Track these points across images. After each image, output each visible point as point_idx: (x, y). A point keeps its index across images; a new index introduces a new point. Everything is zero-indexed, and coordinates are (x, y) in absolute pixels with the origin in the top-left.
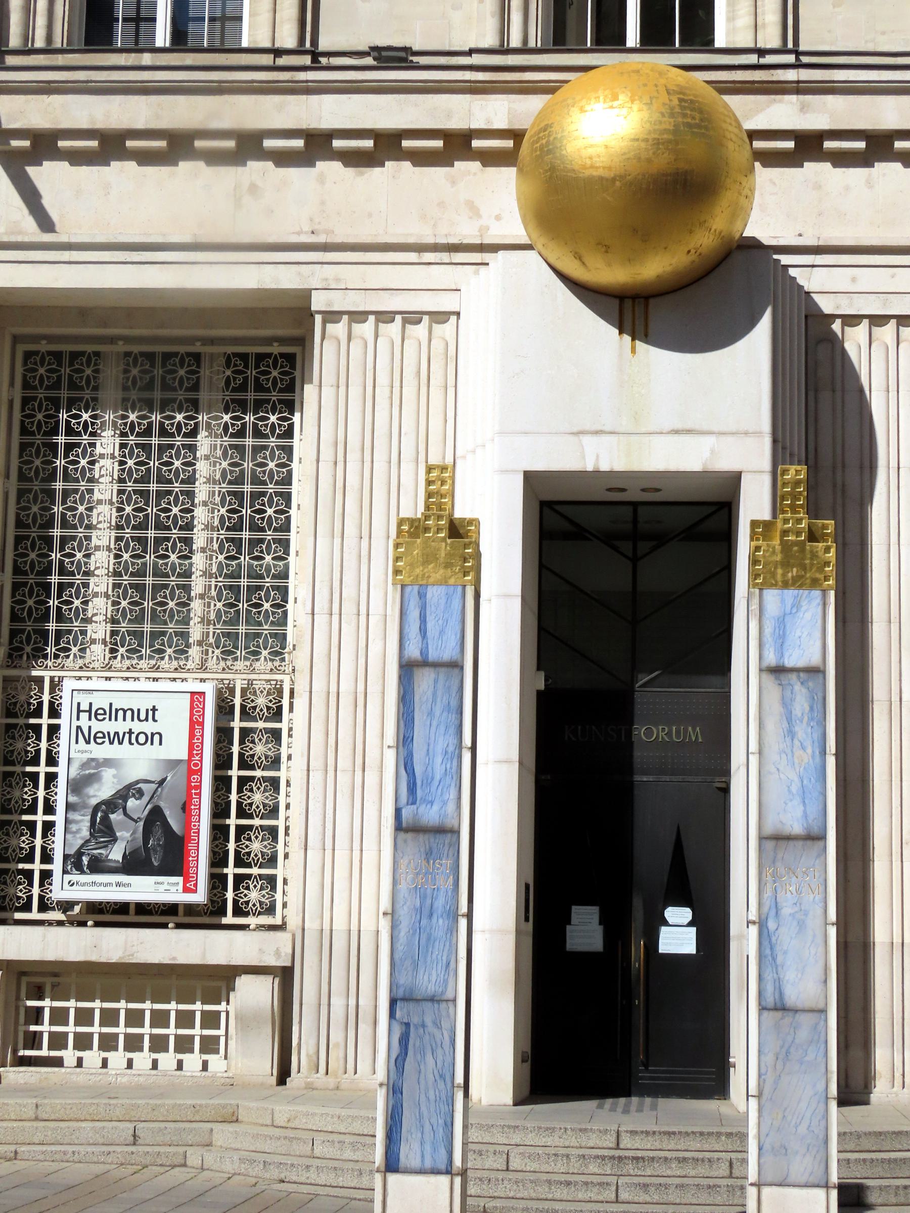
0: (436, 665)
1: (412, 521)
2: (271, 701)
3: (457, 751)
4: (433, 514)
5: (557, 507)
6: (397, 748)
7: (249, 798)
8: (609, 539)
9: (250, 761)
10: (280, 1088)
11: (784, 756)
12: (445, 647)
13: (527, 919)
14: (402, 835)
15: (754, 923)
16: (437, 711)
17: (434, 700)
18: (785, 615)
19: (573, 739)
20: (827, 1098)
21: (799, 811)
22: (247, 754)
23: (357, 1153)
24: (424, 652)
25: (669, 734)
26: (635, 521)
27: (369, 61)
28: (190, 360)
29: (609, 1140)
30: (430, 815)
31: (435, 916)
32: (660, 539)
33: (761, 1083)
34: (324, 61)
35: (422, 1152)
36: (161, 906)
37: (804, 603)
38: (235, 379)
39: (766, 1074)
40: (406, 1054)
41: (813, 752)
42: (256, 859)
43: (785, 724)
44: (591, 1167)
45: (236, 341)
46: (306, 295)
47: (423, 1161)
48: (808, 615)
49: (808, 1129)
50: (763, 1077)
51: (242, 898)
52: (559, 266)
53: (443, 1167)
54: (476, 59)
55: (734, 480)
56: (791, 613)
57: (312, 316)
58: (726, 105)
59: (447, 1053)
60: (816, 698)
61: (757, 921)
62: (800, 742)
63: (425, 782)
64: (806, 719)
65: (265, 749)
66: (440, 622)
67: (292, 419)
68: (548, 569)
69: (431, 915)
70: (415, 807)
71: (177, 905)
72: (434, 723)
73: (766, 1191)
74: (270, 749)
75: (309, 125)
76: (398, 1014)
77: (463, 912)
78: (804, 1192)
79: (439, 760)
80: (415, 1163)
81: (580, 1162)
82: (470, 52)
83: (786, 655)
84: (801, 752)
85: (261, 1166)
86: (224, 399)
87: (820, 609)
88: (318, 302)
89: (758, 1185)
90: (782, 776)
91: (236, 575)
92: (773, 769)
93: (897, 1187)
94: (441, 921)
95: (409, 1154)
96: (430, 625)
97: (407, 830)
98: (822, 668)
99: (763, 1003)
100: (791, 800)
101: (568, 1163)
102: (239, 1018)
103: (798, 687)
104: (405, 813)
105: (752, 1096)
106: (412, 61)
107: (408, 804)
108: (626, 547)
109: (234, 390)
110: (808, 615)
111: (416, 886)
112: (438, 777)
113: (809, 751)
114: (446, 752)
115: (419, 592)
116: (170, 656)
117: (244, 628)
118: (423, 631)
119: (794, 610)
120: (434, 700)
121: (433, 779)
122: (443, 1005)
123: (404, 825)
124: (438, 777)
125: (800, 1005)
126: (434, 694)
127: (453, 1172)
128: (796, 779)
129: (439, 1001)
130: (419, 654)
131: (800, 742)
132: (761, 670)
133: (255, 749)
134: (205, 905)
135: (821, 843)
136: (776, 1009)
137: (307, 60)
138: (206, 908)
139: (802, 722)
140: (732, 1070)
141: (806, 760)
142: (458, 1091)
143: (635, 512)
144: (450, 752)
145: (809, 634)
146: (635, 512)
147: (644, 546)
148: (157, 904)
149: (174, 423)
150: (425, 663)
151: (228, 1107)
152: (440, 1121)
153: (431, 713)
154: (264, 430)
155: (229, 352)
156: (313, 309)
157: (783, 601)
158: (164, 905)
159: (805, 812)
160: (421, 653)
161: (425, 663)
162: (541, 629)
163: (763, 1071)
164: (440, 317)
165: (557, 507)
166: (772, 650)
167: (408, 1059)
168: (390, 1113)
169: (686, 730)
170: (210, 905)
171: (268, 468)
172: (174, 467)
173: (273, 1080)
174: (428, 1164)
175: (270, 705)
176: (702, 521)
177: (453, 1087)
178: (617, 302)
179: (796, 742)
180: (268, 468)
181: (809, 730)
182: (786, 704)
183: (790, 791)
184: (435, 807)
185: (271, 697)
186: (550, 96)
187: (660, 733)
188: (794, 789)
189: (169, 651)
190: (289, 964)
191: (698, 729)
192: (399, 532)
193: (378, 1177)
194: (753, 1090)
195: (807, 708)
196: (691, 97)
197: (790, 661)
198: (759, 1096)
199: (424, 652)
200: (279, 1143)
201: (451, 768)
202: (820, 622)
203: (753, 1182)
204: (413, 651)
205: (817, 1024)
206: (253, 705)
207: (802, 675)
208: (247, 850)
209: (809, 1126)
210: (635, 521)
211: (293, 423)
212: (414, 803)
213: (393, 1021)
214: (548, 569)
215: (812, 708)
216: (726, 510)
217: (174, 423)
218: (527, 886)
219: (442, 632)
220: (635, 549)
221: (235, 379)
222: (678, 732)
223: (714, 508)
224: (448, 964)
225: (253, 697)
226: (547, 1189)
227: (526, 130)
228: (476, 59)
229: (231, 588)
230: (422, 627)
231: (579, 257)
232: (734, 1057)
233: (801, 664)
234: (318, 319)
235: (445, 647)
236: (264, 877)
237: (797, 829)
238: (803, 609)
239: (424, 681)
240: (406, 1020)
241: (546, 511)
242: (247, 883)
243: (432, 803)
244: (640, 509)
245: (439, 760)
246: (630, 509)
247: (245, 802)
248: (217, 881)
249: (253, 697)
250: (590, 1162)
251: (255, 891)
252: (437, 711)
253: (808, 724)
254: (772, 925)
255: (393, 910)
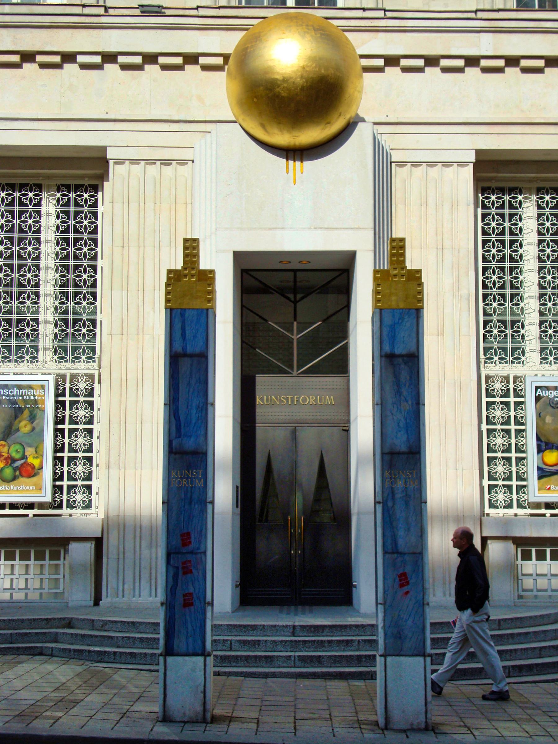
0: (191, 356)
1: (175, 271)
2: (87, 385)
3: (205, 406)
4: (189, 267)
5: (252, 273)
6: (170, 405)
7: (75, 441)
8: (282, 291)
9: (76, 420)
10: (95, 608)
11: (395, 406)
12: (197, 345)
13: (237, 507)
14: (173, 456)
15: (379, 503)
16: (193, 382)
17: (191, 376)
18: (395, 324)
19: (262, 404)
20: (424, 604)
21: (404, 438)
22: (74, 416)
23: (143, 643)
24: (184, 348)
25: (316, 400)
26: (295, 281)
27: (138, 12)
28: (36, 188)
29: (289, 631)
30: (190, 444)
31: (193, 503)
32: (308, 291)
33: (386, 596)
34: (111, 12)
35: (187, 643)
36: (25, 505)
37: (406, 317)
38: (62, 199)
39: (388, 591)
40: (177, 585)
41: (412, 403)
42: (80, 476)
43: (396, 387)
44: (279, 647)
45: (64, 177)
46: (104, 149)
47: (187, 649)
48: (408, 325)
49: (413, 622)
50: (386, 593)
51: (72, 499)
52: (252, 132)
53: (200, 652)
54: (202, 12)
55: (351, 257)
56: (398, 323)
57: (108, 162)
58: (347, 39)
59: (201, 584)
60: (413, 372)
61: (381, 501)
62: (404, 397)
63: (186, 424)
64: (408, 384)
65: (84, 413)
66: (194, 331)
67: (97, 223)
68: (246, 307)
69: (190, 503)
70: (180, 439)
71: (34, 503)
72: (191, 390)
73: (389, 659)
74: (87, 413)
75: (104, 49)
76: (172, 562)
77: (209, 500)
78: (411, 659)
79: (194, 411)
80: (183, 649)
81: (273, 645)
82: (197, 8)
83: (396, 348)
84: (405, 403)
85: (87, 653)
86: (56, 211)
87: (415, 320)
88: (111, 154)
89: (384, 656)
90: (395, 417)
91: (65, 312)
92: (389, 414)
93: (359, 641)
94: (197, 506)
95: (180, 643)
96: (187, 332)
97: (176, 453)
98: (417, 355)
99: (386, 550)
100: (400, 431)
101: (265, 645)
102: (71, 568)
103: (403, 366)
104: (174, 443)
105: (380, 604)
106: (164, 13)
107: (176, 438)
108: (291, 296)
109: (62, 205)
110: (408, 325)
111: (182, 486)
112: (194, 421)
113: (410, 403)
114: (199, 407)
115: (181, 313)
116: (27, 360)
117: (69, 343)
118: (183, 336)
119: (400, 321)
120: (191, 376)
121: (191, 422)
122: (199, 555)
123: (174, 450)
124: (194, 421)
125: (406, 550)
126: (191, 373)
127: (206, 654)
128: (403, 419)
129: (196, 554)
130: (182, 350)
131: (404, 397)
132: (381, 356)
133: (78, 413)
134: (50, 503)
135: (418, 456)
136: (393, 553)
137: (101, 11)
138: (51, 505)
139: (405, 385)
140: (354, 589)
141: (408, 408)
142: (208, 606)
143: (295, 276)
144: (200, 406)
145: (409, 335)
146: (295, 276)
147: (299, 296)
148: (22, 503)
149: (27, 225)
150: (185, 355)
151: (67, 619)
152: (197, 624)
153: (189, 384)
154: (81, 229)
155: (59, 183)
156: (108, 158)
157: (393, 316)
158: (26, 504)
159: (408, 438)
160: (183, 348)
161: (185, 355)
162: (242, 342)
163: (386, 589)
164: (182, 162)
165: (252, 273)
166: (388, 344)
167: (178, 588)
168: (168, 620)
169: (325, 398)
170: (53, 503)
171: (83, 251)
172: (28, 250)
173: (92, 603)
174: (191, 651)
175: (87, 387)
176: (334, 279)
177: (205, 603)
178: (285, 153)
179: (403, 398)
180: (83, 251)
181: (410, 390)
182: (396, 376)
183: (398, 425)
184: (192, 439)
185: (87, 383)
186: (246, 32)
187: (311, 400)
188: (401, 425)
189: (27, 357)
190: (100, 536)
191: (332, 397)
192: (168, 278)
193: (161, 659)
194: (380, 600)
195: (408, 378)
196: (327, 33)
197: (398, 351)
198: (384, 604)
199: (184, 348)
200: (97, 640)
201: (201, 416)
202: (415, 328)
203: (382, 654)
204: (178, 347)
205: (417, 561)
206: (77, 387)
207: (405, 358)
208: (74, 471)
209: (413, 621)
210: (295, 281)
211: (97, 225)
212: (180, 437)
213: (169, 566)
214: (246, 307)
215: (411, 378)
216: (346, 274)
217: (27, 225)
218: (237, 487)
219: (195, 337)
220: (295, 297)
221: (62, 199)
222: (321, 399)
223: (337, 273)
224: (201, 531)
225: (77, 383)
226: (254, 661)
227: (230, 54)
228: (202, 12)
229: (62, 320)
230: (183, 333)
231: (263, 126)
232: (356, 582)
233: (404, 352)
234: (111, 163)
235: (197, 345)
236: (84, 486)
237: (404, 448)
238: (406, 320)
239: (185, 365)
240: (176, 565)
241: (244, 274)
242: (75, 490)
243: (190, 437)
244: (299, 274)
245: (194, 411)
246: (291, 274)
247: (73, 443)
248: (57, 489)
249: (77, 383)
250: (278, 644)
251: (79, 494)
252: (193, 382)
253: (409, 386)
254: (390, 504)
255: (168, 500)
